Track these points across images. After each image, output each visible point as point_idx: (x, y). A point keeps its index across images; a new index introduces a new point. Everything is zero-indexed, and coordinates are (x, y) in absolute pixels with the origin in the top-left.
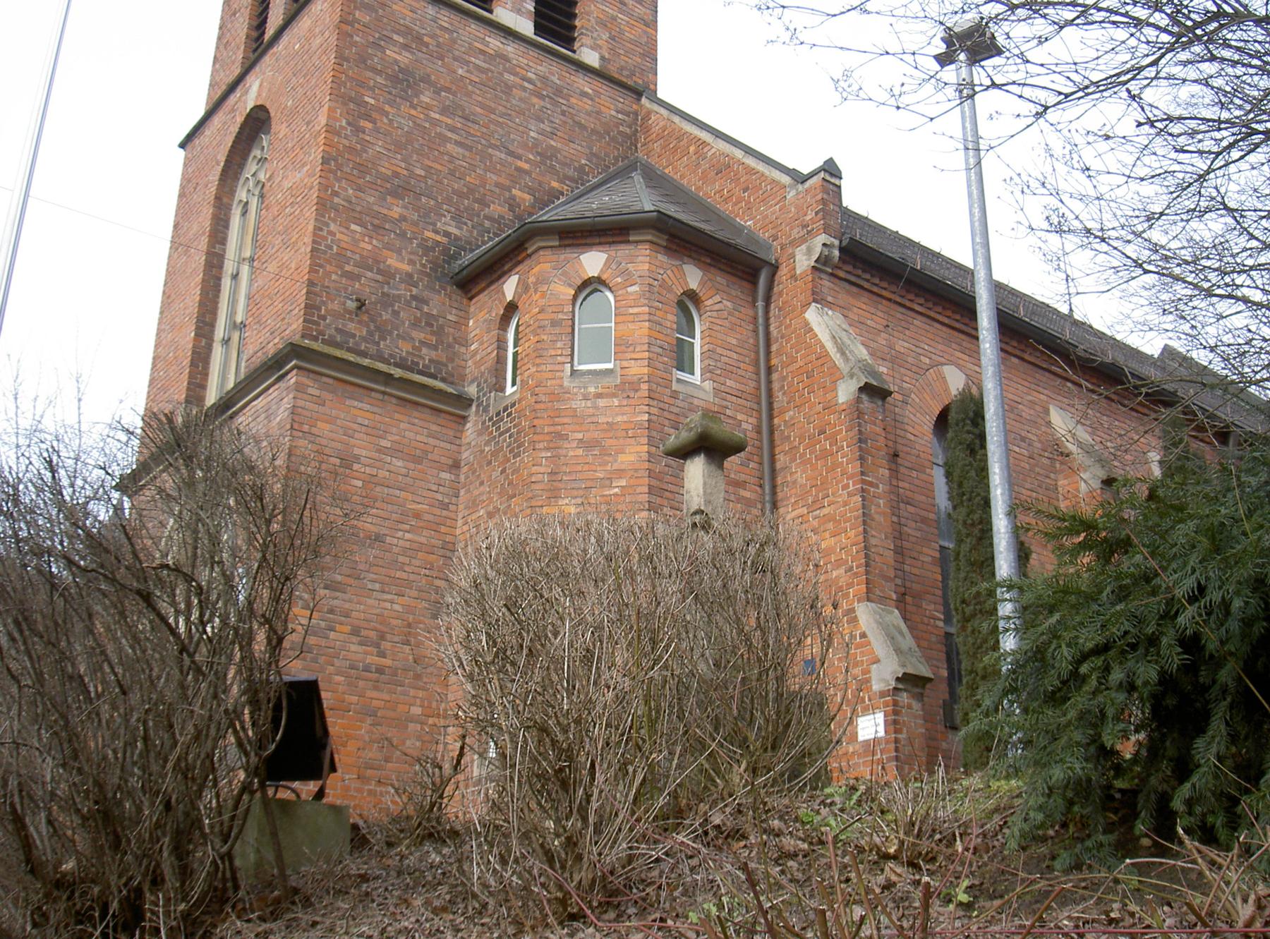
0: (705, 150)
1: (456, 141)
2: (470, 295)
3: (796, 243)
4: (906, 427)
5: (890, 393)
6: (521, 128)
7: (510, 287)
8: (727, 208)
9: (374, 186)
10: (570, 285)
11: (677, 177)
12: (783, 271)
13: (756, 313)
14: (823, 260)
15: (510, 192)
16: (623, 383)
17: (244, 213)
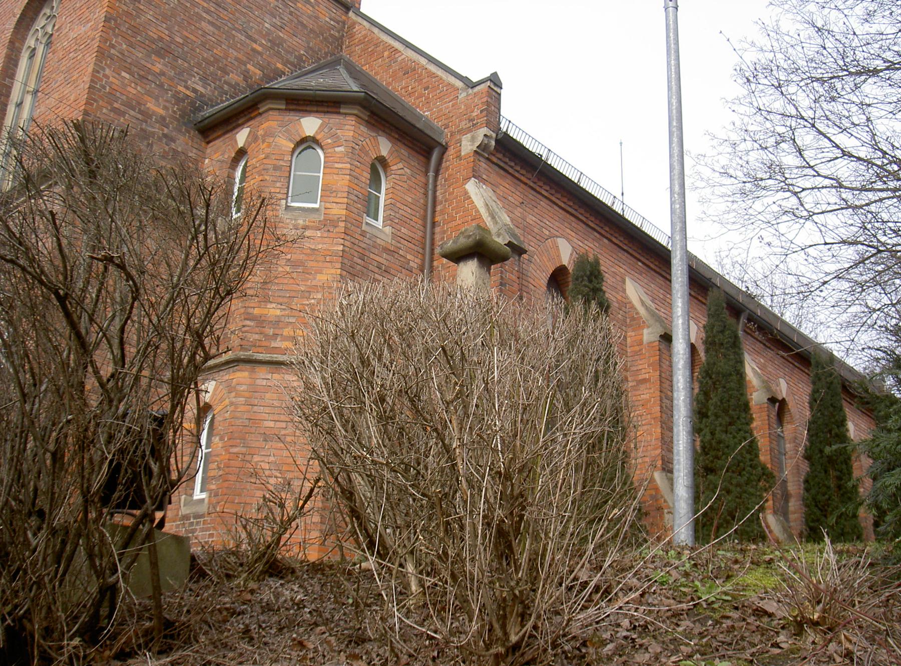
0: (397, 56)
1: (209, 20)
2: (207, 140)
3: (462, 132)
4: (530, 280)
5: (525, 252)
6: (258, 20)
7: (242, 137)
8: (410, 101)
9: (143, 45)
10: (290, 140)
11: (372, 73)
12: (451, 152)
13: (428, 181)
14: (482, 147)
15: (245, 65)
16: (325, 220)
17: (32, 56)
